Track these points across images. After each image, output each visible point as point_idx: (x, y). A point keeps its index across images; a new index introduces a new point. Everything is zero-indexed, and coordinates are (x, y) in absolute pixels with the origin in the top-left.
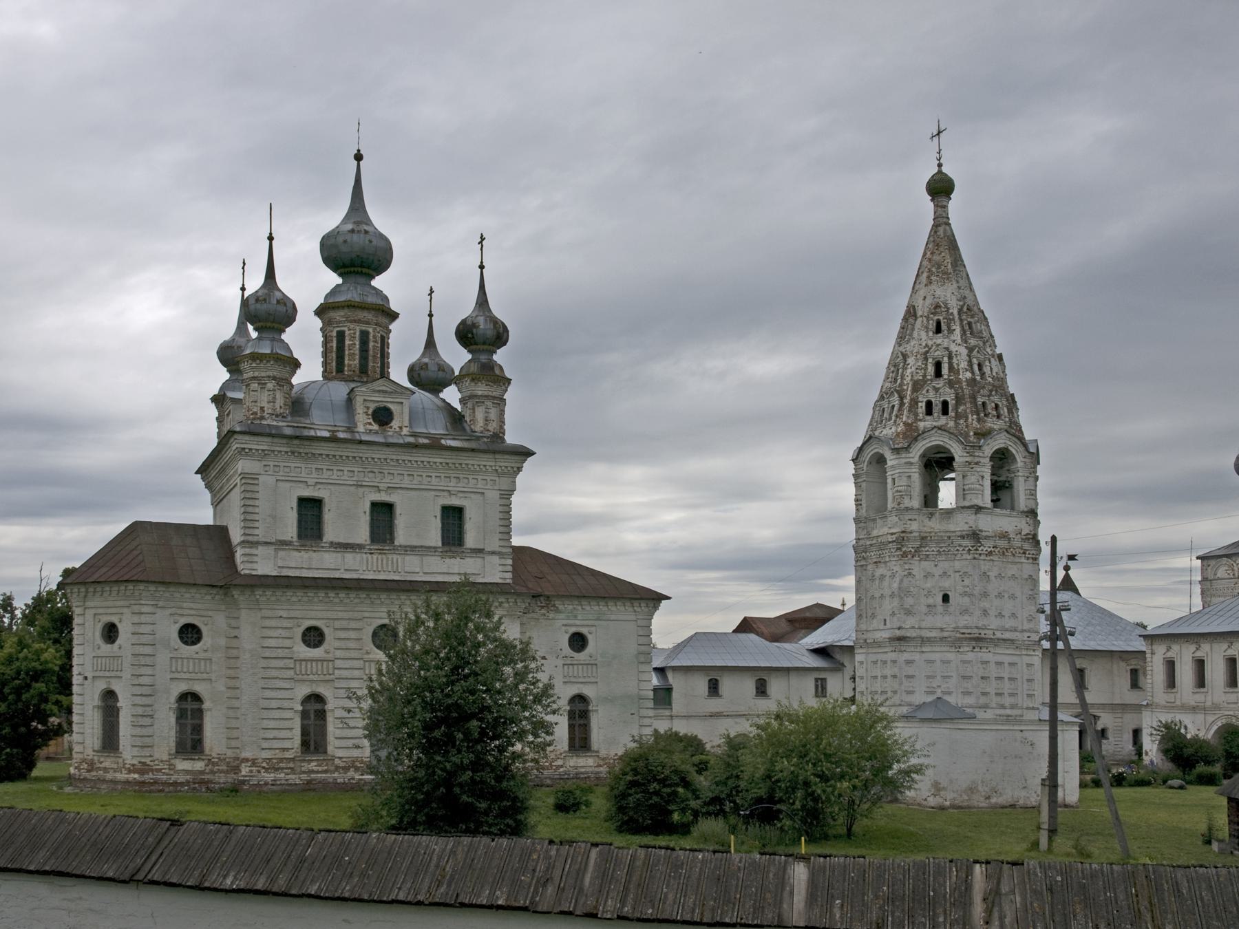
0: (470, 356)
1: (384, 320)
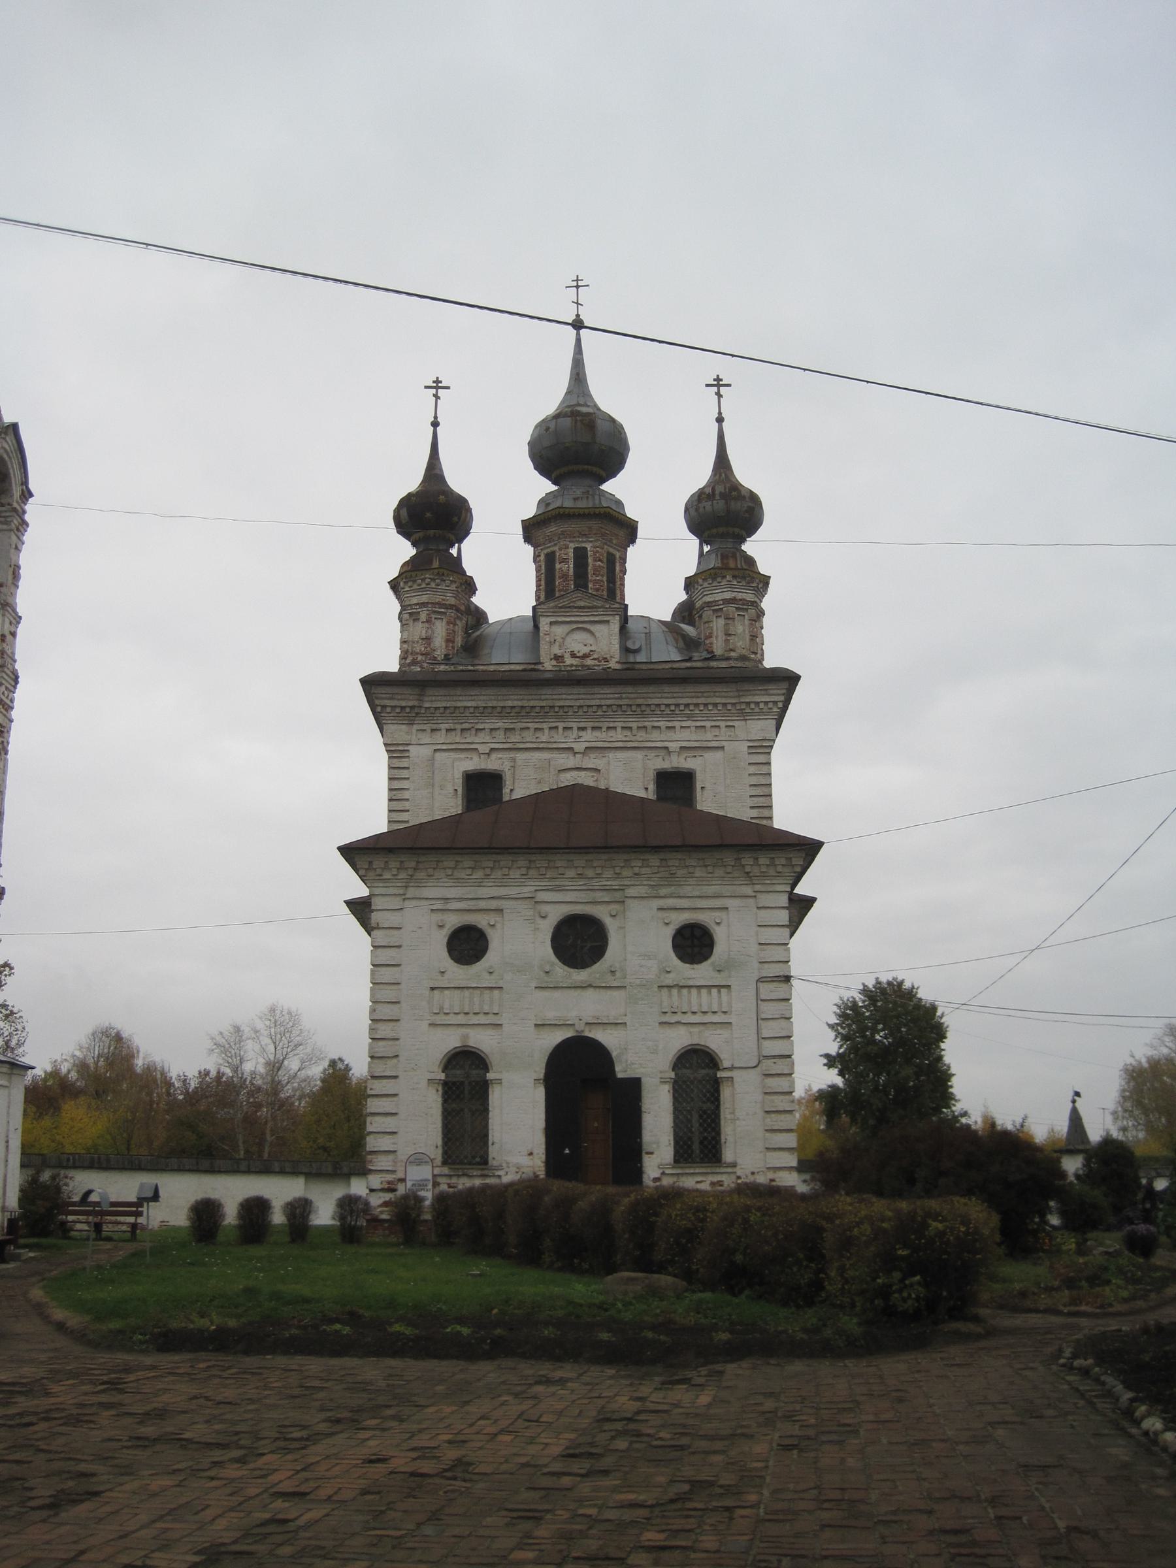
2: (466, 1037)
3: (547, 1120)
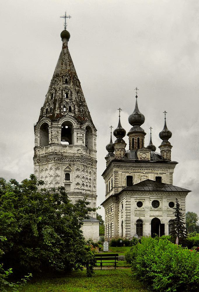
0: (162, 141)
1: (143, 135)
2: (140, 218)
3: (151, 230)
